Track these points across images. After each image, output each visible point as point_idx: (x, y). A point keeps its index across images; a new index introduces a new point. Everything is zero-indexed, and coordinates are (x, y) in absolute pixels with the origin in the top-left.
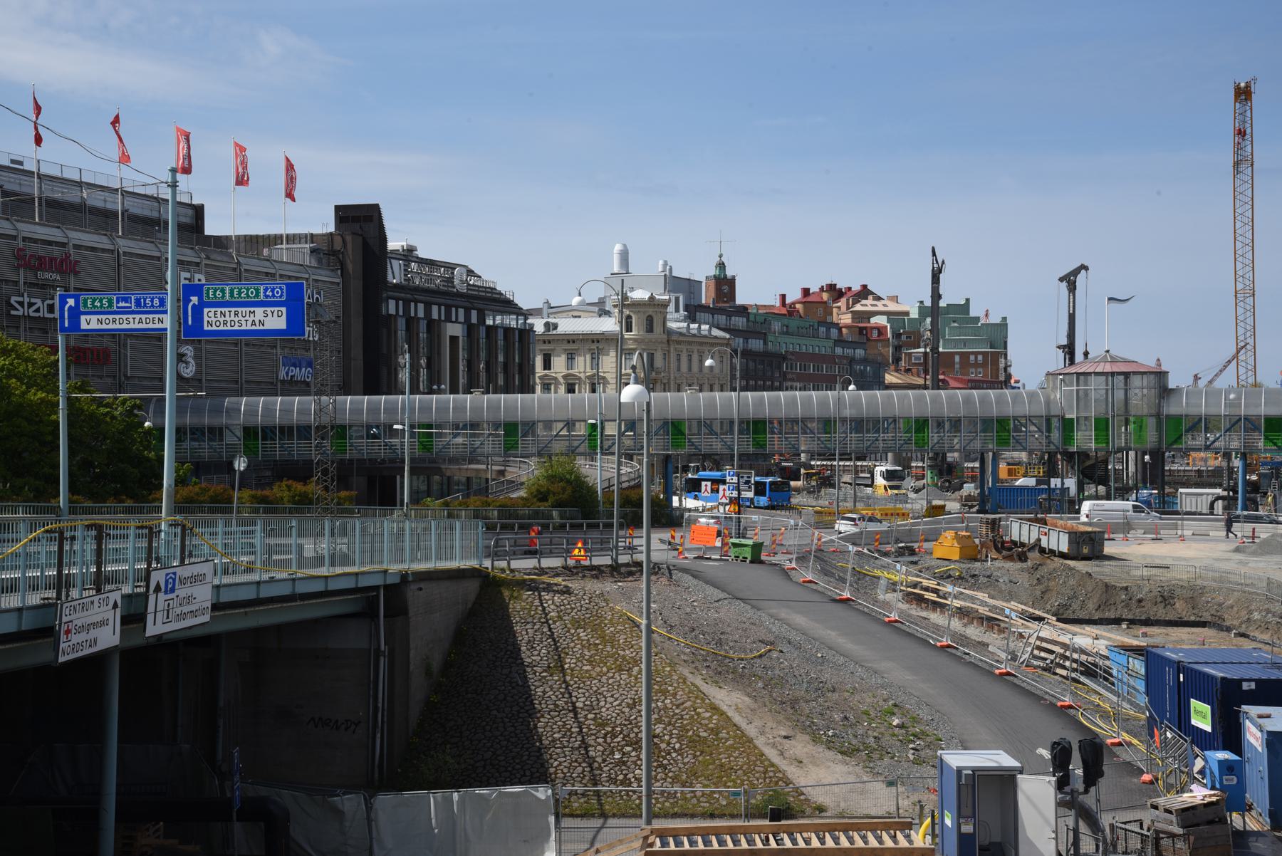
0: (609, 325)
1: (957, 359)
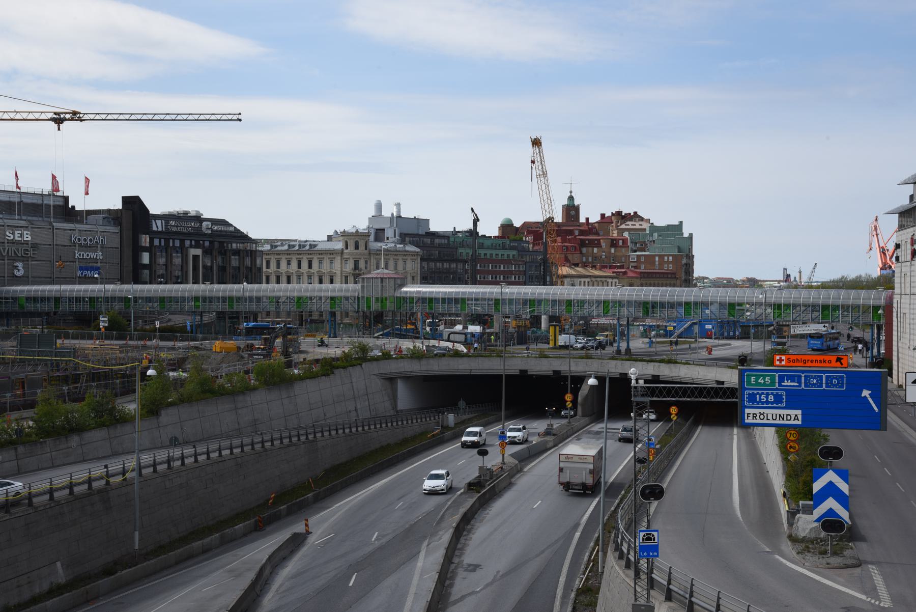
0: (339, 246)
1: (657, 259)
